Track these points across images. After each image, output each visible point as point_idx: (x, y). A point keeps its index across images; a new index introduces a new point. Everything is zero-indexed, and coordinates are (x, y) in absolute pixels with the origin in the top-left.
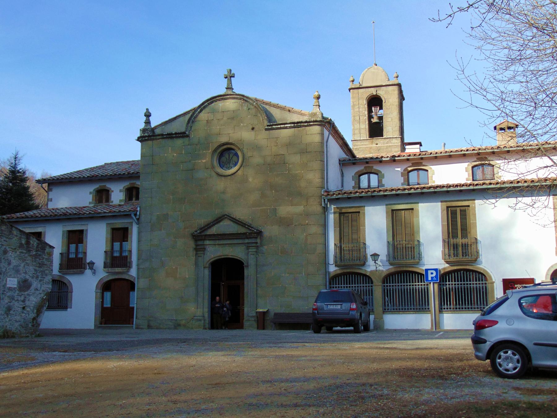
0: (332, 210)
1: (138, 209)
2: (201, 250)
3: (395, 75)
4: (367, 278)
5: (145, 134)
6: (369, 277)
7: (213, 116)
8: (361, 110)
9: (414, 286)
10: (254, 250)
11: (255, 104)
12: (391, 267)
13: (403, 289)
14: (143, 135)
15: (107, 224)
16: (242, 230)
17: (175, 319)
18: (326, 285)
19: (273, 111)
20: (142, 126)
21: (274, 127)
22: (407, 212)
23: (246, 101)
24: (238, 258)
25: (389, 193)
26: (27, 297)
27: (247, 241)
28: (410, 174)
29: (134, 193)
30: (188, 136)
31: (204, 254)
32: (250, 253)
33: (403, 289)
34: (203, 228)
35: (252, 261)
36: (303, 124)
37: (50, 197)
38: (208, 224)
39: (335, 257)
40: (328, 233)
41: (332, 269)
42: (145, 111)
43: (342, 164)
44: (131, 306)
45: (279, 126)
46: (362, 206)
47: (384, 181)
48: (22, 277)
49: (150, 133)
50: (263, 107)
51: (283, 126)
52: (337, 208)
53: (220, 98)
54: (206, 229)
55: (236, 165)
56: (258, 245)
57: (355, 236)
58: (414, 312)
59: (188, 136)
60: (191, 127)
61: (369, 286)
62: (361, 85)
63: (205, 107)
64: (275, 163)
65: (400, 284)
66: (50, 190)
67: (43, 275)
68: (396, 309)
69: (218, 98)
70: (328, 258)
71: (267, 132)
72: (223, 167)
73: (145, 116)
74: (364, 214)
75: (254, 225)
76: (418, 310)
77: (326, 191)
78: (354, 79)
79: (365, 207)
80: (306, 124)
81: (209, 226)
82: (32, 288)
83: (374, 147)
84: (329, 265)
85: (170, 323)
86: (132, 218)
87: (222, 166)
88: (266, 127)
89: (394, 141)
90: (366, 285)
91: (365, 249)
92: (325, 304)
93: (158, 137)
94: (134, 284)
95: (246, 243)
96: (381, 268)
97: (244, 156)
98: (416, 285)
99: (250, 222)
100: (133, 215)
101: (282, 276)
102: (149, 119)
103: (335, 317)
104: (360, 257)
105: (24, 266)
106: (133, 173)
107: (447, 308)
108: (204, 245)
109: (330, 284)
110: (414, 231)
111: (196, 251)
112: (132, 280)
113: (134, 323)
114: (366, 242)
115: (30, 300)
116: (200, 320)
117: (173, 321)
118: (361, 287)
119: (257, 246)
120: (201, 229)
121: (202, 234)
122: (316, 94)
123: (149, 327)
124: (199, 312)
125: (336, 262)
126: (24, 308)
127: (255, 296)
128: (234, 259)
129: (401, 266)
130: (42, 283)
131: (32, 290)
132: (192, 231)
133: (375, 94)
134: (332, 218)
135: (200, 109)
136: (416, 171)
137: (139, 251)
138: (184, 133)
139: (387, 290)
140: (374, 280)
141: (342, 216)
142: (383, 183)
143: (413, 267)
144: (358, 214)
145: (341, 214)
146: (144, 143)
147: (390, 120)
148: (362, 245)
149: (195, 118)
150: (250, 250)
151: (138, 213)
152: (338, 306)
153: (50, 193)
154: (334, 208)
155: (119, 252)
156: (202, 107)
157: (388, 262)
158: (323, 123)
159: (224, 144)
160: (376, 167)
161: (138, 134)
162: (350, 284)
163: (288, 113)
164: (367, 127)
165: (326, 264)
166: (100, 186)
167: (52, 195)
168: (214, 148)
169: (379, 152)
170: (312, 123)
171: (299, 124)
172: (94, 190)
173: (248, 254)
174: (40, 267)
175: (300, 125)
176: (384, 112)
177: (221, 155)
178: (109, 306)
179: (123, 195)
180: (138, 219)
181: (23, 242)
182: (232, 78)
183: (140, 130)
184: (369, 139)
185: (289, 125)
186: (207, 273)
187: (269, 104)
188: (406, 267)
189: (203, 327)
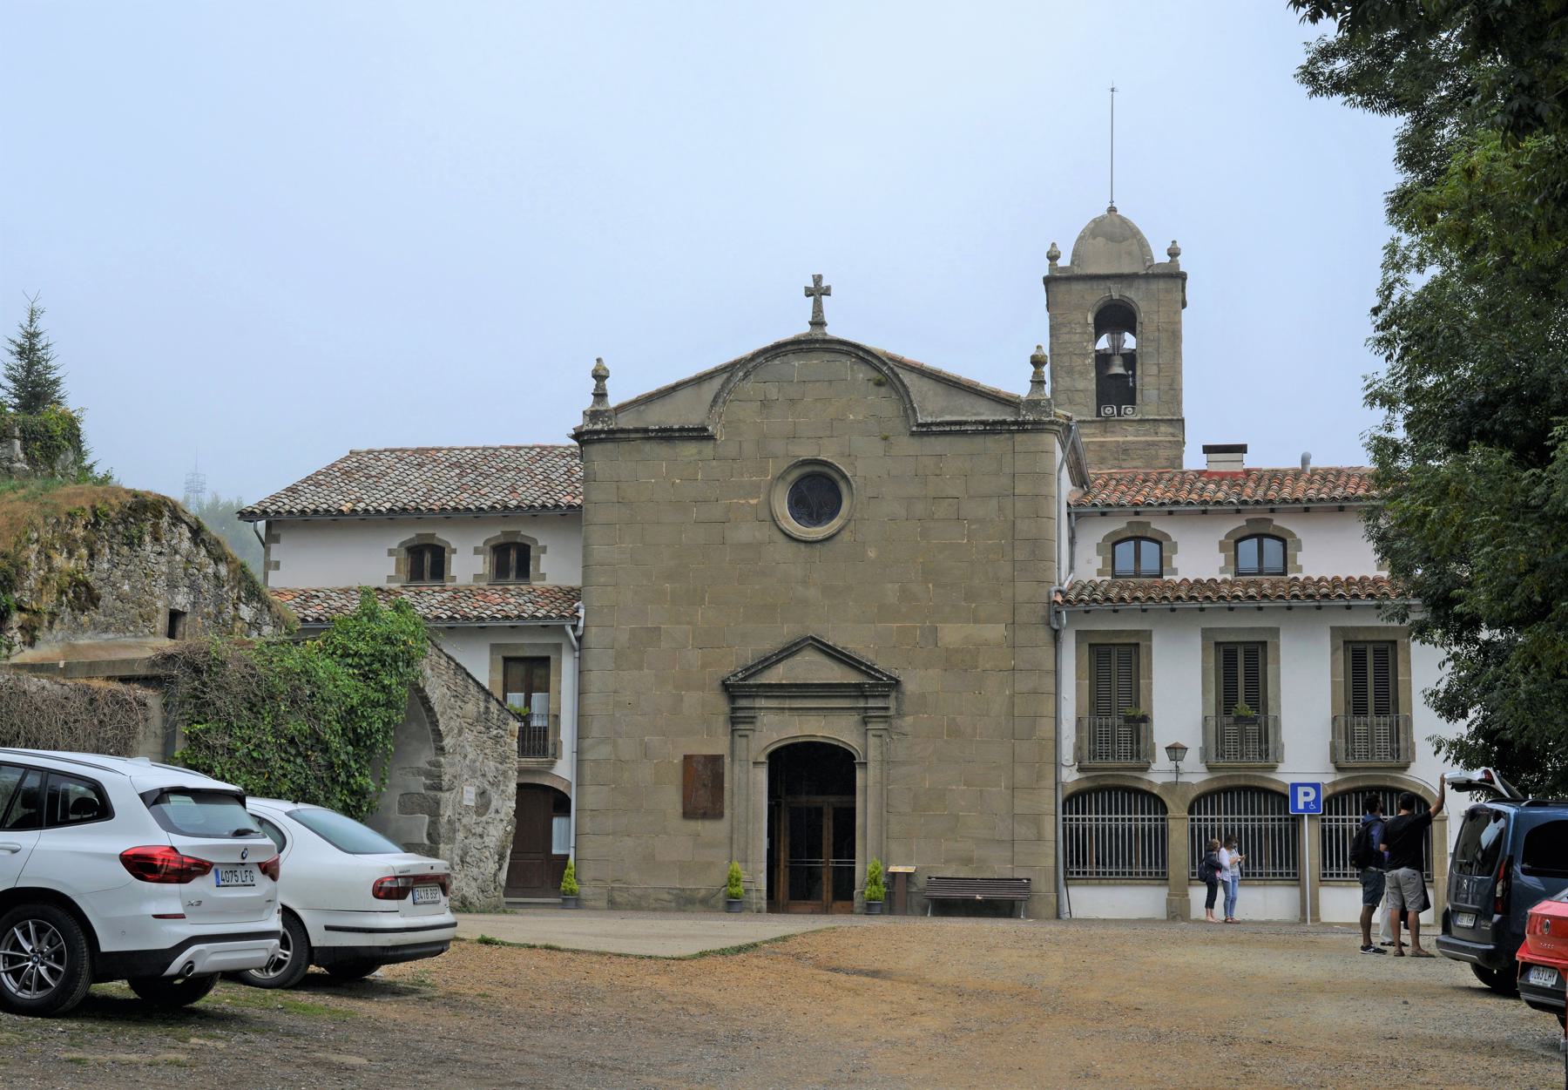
1: (581, 613)
2: (747, 720)
4: (1154, 802)
5: (595, 424)
6: (1158, 799)
9: (1216, 823)
14: (590, 427)
16: (853, 678)
20: (588, 402)
21: (934, 429)
23: (862, 359)
27: (861, 704)
29: (513, 556)
32: (870, 733)
34: (752, 666)
35: (873, 754)
37: (274, 557)
38: (766, 659)
41: (1070, 776)
42: (593, 365)
43: (1076, 513)
51: (958, 428)
54: (761, 671)
55: (833, 514)
56: (891, 713)
61: (1156, 820)
64: (936, 517)
65: (1127, 816)
66: (270, 539)
69: (789, 348)
74: (1150, 648)
76: (1271, 877)
81: (767, 663)
88: (914, 429)
94: (569, 801)
101: (951, 790)
107: (1338, 875)
109: (1064, 813)
111: (733, 724)
112: (561, 789)
117: (675, 892)
118: (1090, 820)
120: (747, 670)
121: (751, 682)
125: (1078, 759)
128: (833, 745)
130: (503, 796)
136: (1256, 540)
137: (582, 718)
142: (1174, 566)
150: (870, 726)
151: (581, 624)
153: (274, 547)
161: (578, 421)
162: (1084, 813)
165: (1057, 765)
166: (418, 535)
167: (276, 552)
172: (401, 545)
179: (484, 563)
180: (579, 639)
183: (584, 412)
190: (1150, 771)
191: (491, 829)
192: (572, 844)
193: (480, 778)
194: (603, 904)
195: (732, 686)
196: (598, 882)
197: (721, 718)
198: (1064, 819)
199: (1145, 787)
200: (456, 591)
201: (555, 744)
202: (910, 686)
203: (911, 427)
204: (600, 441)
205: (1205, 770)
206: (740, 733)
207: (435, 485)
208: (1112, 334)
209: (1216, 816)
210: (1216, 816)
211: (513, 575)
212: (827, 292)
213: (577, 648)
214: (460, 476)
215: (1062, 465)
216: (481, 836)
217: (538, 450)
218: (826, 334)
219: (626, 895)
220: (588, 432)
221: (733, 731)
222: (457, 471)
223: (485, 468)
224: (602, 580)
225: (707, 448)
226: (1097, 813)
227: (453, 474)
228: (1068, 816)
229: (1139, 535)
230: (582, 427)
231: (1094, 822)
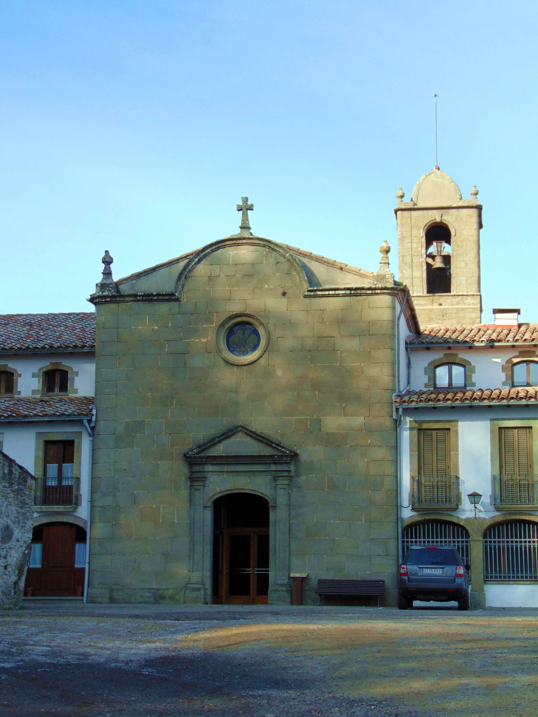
0: (406, 425)
1: (94, 412)
2: (200, 479)
3: (473, 190)
5: (103, 292)
6: (463, 528)
7: (219, 270)
8: (414, 245)
10: (286, 482)
11: (288, 255)
12: (498, 513)
13: (514, 547)
14: (101, 293)
15: (38, 433)
16: (267, 451)
17: (155, 587)
18: (398, 539)
19: (316, 268)
20: (99, 278)
21: (319, 293)
22: (521, 431)
23: (273, 249)
24: (259, 494)
25: (497, 404)
26: (9, 550)
27: (273, 468)
28: (516, 368)
29: (58, 379)
30: (177, 300)
31: (204, 486)
33: (514, 547)
34: (203, 445)
35: (281, 498)
36: (364, 292)
38: (212, 440)
39: (412, 495)
40: (400, 460)
42: (103, 254)
44: (77, 566)
45: (327, 293)
46: (453, 421)
47: (475, 378)
48: (4, 523)
49: (113, 291)
50: (300, 260)
51: (333, 292)
52: (416, 421)
53: (231, 242)
54: (208, 448)
55: (255, 348)
56: (292, 474)
57: (442, 466)
58: (532, 582)
59: (177, 300)
60: (183, 286)
62: (415, 204)
63: (205, 256)
65: (497, 540)
67: (24, 520)
68: (505, 577)
69: (227, 243)
70: (401, 497)
71: (307, 300)
72: (234, 350)
73: (103, 262)
74: (456, 432)
75: (285, 442)
77: (398, 396)
78: (404, 194)
79: (457, 421)
80: (370, 292)
81: (213, 442)
82: (14, 538)
83: (436, 309)
84: (402, 508)
85: (147, 594)
86: (84, 426)
87: (232, 349)
88: (306, 293)
89: (470, 300)
90: (458, 540)
91: (458, 485)
92: (420, 566)
93: (127, 299)
95: (272, 471)
96: (482, 515)
97: (269, 335)
98: (525, 542)
99: (279, 438)
100: (85, 422)
102: (110, 268)
103: (433, 585)
104: (450, 497)
105: (7, 507)
106: (59, 347)
108: (204, 472)
109: (403, 537)
110: (532, 462)
113: (85, 594)
114: (459, 475)
115: (12, 555)
116: (198, 589)
117: (153, 591)
119: (291, 476)
120: (199, 447)
121: (202, 455)
122: (385, 245)
123: (112, 600)
124: (196, 577)
126: (5, 567)
127: (287, 554)
129: (513, 513)
130: (23, 530)
131: (13, 541)
132: (185, 449)
133: (438, 220)
134: (406, 435)
135: (199, 258)
136: (525, 364)
137: (93, 478)
138: (173, 295)
139: (491, 548)
140: (470, 532)
141: (422, 434)
143: (530, 515)
144: (446, 432)
145: (420, 432)
146: (104, 306)
147: (462, 265)
148: (453, 480)
149: (190, 271)
150: (279, 482)
151: (94, 419)
152: (438, 571)
154: (410, 421)
155: (57, 480)
156: (202, 254)
157: (493, 506)
158: (396, 292)
159: (237, 316)
160: (463, 356)
161: (93, 290)
163: (339, 271)
164: (425, 275)
165: (398, 507)
168: (222, 321)
169: (444, 318)
170: (379, 291)
171: (359, 292)
173: (276, 488)
174: (21, 508)
175: (361, 293)
176: (453, 250)
177: (230, 332)
178: (39, 566)
179: (39, 382)
180: (93, 428)
181: (6, 471)
182: (249, 211)
183: (97, 285)
184: (428, 295)
185: (343, 292)
186: (208, 515)
187: (309, 256)
188: (516, 514)
189: (202, 600)
190: (458, 510)
191: (13, 553)
192: (87, 561)
193: (5, 519)
194: (106, 599)
195: (190, 457)
196: (102, 586)
197: (183, 479)
198: (403, 542)
199: (455, 520)
200: (19, 400)
201: (77, 497)
202: (304, 457)
203: (304, 292)
204: (107, 302)
205: (494, 510)
206: (195, 487)
207: (11, 335)
208: (437, 243)
209: (448, 540)
210: (501, 540)
211: (57, 389)
212: (251, 208)
213: (91, 435)
214: (29, 330)
215: (400, 313)
216: (5, 557)
217: (82, 315)
218: (251, 234)
219: (121, 593)
220: (99, 297)
221: (191, 486)
222: (28, 327)
223: (46, 325)
224: (108, 391)
225: (175, 305)
226: (424, 538)
227: (24, 329)
228: (406, 540)
229: (451, 361)
230: (95, 294)
231: (497, 544)
